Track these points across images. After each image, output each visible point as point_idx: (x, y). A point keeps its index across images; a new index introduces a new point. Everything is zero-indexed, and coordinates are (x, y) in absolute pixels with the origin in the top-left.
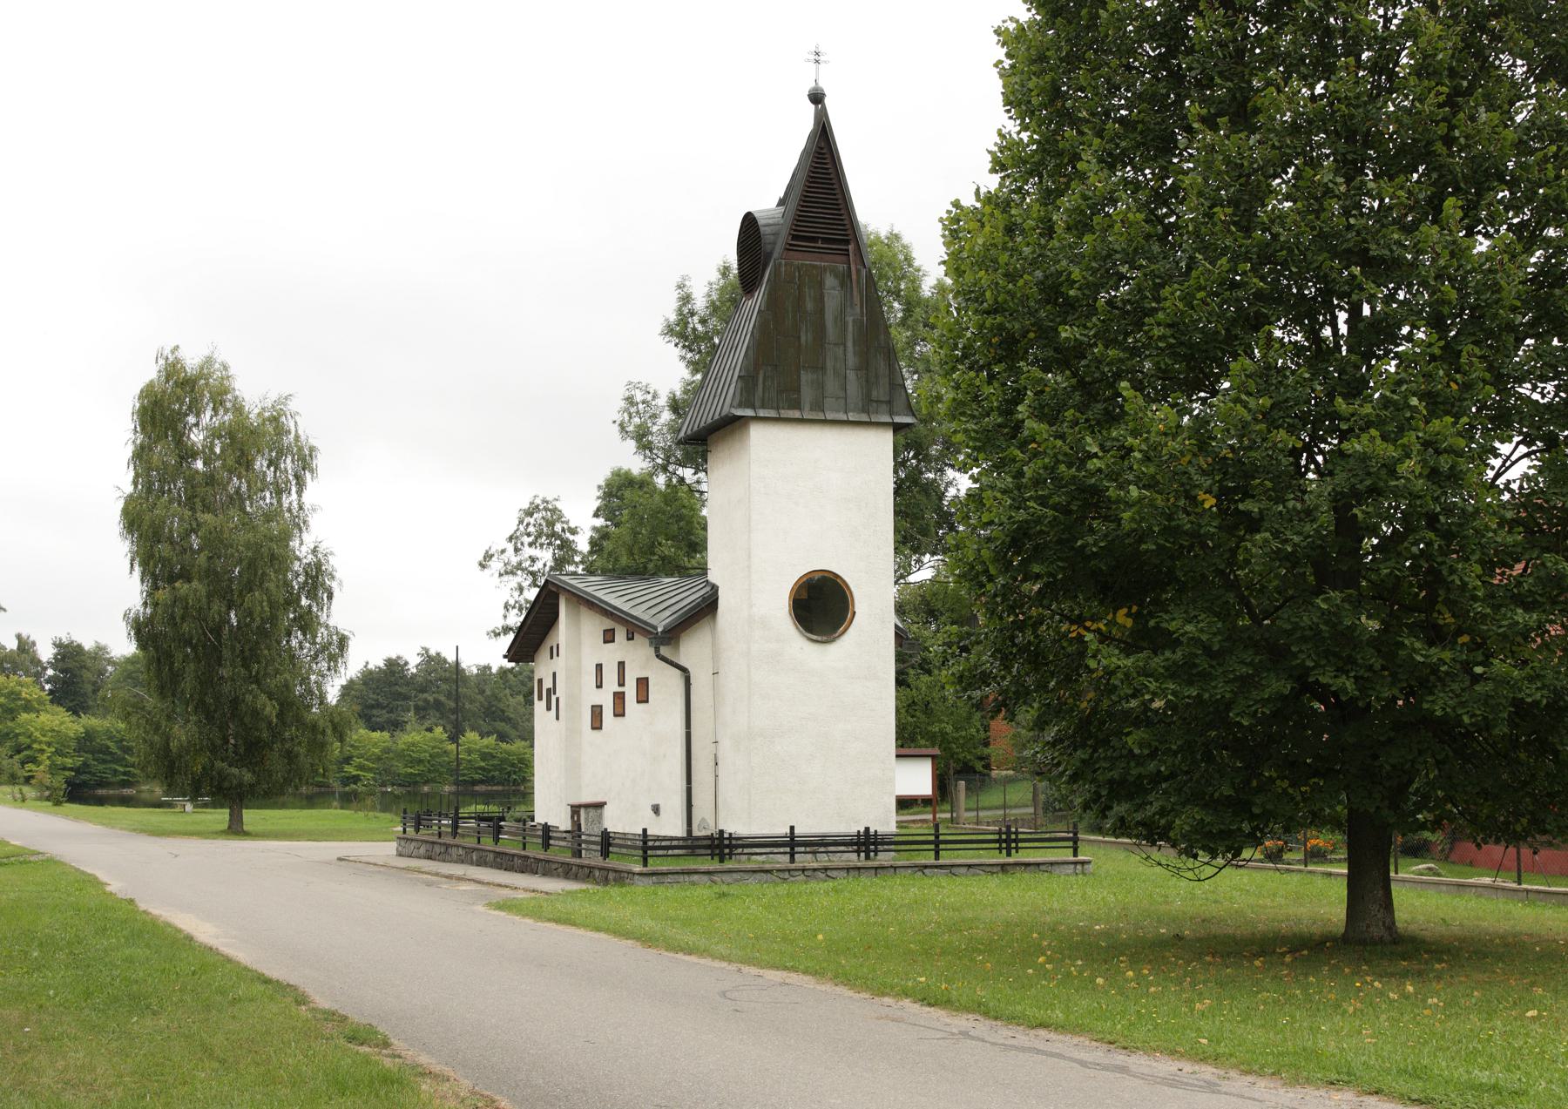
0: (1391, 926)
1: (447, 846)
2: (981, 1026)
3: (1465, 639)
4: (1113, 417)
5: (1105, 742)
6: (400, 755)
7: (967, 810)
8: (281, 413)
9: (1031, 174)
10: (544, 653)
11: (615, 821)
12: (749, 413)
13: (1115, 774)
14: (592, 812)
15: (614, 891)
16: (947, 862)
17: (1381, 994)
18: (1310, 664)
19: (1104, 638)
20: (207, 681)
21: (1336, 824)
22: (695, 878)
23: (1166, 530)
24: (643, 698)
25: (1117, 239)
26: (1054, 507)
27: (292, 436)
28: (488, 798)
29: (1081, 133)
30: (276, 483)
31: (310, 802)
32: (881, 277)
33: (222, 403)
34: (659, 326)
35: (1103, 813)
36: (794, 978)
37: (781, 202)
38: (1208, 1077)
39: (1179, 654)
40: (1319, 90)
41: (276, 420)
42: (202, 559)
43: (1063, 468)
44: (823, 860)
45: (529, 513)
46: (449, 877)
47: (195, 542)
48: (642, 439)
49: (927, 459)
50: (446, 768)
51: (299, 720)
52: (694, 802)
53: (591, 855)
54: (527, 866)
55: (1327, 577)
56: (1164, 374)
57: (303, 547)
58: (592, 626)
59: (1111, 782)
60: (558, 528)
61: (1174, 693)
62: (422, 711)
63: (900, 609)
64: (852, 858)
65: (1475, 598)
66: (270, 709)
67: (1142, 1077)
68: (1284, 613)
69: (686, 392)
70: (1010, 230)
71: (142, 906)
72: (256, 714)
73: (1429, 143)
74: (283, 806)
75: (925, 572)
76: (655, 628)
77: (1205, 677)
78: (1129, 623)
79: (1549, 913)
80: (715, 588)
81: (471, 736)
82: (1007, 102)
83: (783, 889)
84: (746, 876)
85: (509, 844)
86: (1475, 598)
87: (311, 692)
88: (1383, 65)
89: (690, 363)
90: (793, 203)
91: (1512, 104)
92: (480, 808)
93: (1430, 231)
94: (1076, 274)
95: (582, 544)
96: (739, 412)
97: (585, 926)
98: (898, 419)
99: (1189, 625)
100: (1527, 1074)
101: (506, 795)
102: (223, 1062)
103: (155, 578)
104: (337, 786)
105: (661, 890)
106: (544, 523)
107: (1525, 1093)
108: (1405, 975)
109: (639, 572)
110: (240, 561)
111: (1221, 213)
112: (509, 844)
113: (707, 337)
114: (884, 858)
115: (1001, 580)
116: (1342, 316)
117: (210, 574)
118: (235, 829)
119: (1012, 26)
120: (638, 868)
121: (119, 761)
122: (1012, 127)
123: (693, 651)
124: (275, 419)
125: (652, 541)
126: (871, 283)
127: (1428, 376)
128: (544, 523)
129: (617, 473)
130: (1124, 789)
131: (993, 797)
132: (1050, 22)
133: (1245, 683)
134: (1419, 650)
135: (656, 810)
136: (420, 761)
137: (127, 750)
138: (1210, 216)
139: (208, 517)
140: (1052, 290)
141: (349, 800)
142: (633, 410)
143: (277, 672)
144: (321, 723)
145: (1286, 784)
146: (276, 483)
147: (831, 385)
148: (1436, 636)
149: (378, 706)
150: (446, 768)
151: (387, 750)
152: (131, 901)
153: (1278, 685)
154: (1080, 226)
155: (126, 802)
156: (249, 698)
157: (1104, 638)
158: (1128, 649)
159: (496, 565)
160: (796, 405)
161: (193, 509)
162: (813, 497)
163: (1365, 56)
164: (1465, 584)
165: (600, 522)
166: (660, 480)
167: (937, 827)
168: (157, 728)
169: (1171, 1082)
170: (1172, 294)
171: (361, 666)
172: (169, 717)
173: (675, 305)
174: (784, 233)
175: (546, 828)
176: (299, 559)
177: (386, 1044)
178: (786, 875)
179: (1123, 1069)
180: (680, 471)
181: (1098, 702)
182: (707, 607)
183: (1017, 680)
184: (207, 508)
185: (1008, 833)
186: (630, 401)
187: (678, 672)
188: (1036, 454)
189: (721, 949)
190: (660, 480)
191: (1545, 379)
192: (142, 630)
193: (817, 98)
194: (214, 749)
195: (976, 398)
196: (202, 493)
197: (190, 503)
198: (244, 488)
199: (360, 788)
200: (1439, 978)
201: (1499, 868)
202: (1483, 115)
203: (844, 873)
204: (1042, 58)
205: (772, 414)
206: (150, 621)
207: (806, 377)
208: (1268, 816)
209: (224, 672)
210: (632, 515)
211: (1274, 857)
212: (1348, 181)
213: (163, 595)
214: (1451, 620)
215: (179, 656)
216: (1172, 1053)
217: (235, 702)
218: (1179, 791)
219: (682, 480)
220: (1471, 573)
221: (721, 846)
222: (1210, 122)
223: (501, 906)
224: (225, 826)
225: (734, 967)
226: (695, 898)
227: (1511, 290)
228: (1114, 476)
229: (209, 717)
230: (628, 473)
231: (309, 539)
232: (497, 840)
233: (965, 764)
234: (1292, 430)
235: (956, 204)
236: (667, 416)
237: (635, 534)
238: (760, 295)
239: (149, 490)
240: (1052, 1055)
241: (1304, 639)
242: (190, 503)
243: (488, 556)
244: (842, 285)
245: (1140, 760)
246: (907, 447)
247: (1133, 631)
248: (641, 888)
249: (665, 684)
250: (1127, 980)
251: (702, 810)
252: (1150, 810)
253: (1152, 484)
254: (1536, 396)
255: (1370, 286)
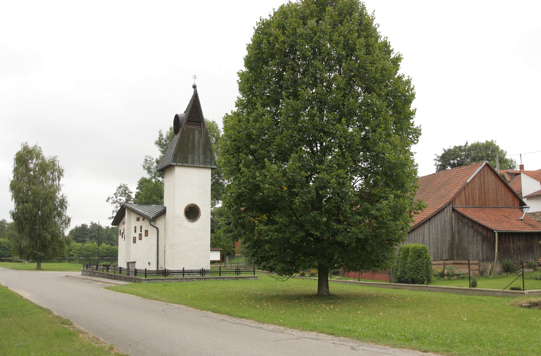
0: (328, 292)
1: (95, 273)
2: (227, 318)
3: (346, 223)
4: (263, 167)
5: (260, 247)
6: (85, 249)
8: (55, 160)
9: (245, 108)
10: (121, 224)
11: (138, 266)
12: (175, 164)
13: (262, 255)
14: (132, 264)
15: (137, 284)
17: (325, 308)
18: (309, 229)
19: (260, 222)
20: (32, 229)
21: (314, 267)
23: (274, 196)
24: (146, 235)
25: (265, 125)
26: (248, 189)
28: (108, 260)
29: (257, 98)
30: (52, 178)
31: (60, 261)
32: (210, 131)
33: (39, 157)
34: (154, 142)
35: (260, 264)
36: (181, 306)
37: (185, 112)
38: (282, 329)
39: (278, 226)
40: (314, 91)
41: (53, 163)
42: (31, 198)
43: (250, 179)
44: (192, 276)
45: (120, 188)
46: (95, 281)
47: (30, 193)
48: (149, 170)
49: (221, 177)
50: (96, 252)
51: (57, 240)
52: (159, 261)
53: (132, 275)
54: (115, 278)
55: (314, 208)
56: (276, 158)
57: (59, 195)
58: (134, 217)
59: (261, 257)
60: (127, 192)
61: (277, 236)
62: (91, 238)
63: (213, 214)
64: (199, 276)
65: (348, 213)
66: (49, 237)
67: (266, 330)
68: (303, 216)
69: (160, 158)
70: (239, 121)
71: (10, 289)
72: (45, 238)
73: (339, 105)
74: (53, 262)
75: (219, 205)
77: (284, 232)
78: (266, 218)
79: (365, 288)
80: (165, 208)
81: (104, 245)
82: (240, 90)
83: (181, 284)
85: (111, 272)
86: (348, 213)
87: (60, 233)
88: (329, 87)
89: (162, 151)
90: (188, 113)
91: (358, 98)
92: (105, 263)
93: (339, 126)
94: (254, 132)
95: (133, 196)
96: (173, 164)
97: (129, 293)
98: (212, 167)
99: (281, 219)
100: (357, 327)
101: (112, 259)
102: (26, 330)
103: (18, 202)
104: (67, 257)
105: (150, 284)
106: (124, 190)
107: (356, 331)
108: (331, 303)
109: (147, 204)
110: (42, 198)
111: (290, 119)
112: (111, 272)
113: (166, 145)
114: (207, 276)
115: (235, 207)
116: (319, 145)
117: (34, 202)
118: (39, 268)
119: (241, 72)
120: (144, 278)
121: (8, 250)
122: (241, 96)
123: (159, 223)
124: (53, 162)
125: (151, 195)
126: (206, 131)
127: (338, 160)
128: (124, 190)
129: (143, 178)
130: (263, 259)
131: (235, 261)
132: (250, 72)
133: (294, 233)
134: (335, 226)
135: (149, 263)
136: (90, 251)
137: (10, 247)
138: (287, 120)
139: (34, 187)
140: (249, 136)
141: (70, 261)
143: (51, 227)
144: (63, 241)
145: (303, 258)
146: (52, 178)
147: (196, 158)
148: (339, 222)
149: (79, 236)
150: (96, 252)
151: (82, 248)
152: (7, 287)
153: (302, 234)
154: (256, 121)
155: (10, 261)
156: (43, 234)
157: (260, 222)
158: (266, 224)
159: (111, 201)
160: (187, 162)
161: (30, 185)
162: (191, 185)
163: (324, 84)
164: (345, 210)
165: (138, 191)
166: (154, 180)
167: (220, 268)
168: (18, 241)
169: (273, 331)
170: (278, 138)
171: (75, 226)
172: (21, 239)
173: (158, 137)
174: (185, 120)
175: (121, 268)
177: (72, 324)
179: (261, 328)
180: (158, 178)
181: (259, 237)
182: (163, 212)
183: (238, 232)
184: (33, 184)
185: (238, 269)
186: (146, 160)
188: (244, 176)
189: (164, 299)
190: (154, 180)
191: (365, 162)
192: (14, 215)
193: (194, 87)
194: (33, 247)
195: (229, 162)
196: (32, 181)
197: (29, 183)
198: (44, 179)
199: (73, 258)
200: (339, 304)
201: (355, 278)
202: (351, 100)
204: (248, 80)
205: (181, 164)
206: (17, 213)
207: (190, 156)
208: (299, 266)
209: (37, 227)
210: (146, 189)
211: (303, 275)
212: (320, 113)
213: (21, 207)
214: (342, 218)
215: (24, 223)
216: (274, 324)
217: (40, 235)
218: (278, 259)
219: (159, 180)
220: (347, 207)
221: (165, 273)
222: (288, 97)
223: (107, 288)
224: (36, 267)
225: (166, 303)
226: (159, 286)
227: (357, 140)
228: (262, 182)
229: (32, 239)
230: (146, 178)
231: (61, 193)
232: (108, 271)
234: (306, 172)
235: (227, 114)
236: (155, 164)
237: (147, 194)
238: (179, 135)
239: (18, 179)
240: (244, 325)
241: (308, 223)
242: (29, 183)
243: (109, 199)
244: (200, 133)
245: (268, 252)
246: (216, 174)
247: (267, 221)
248: (144, 284)
249: (152, 232)
250: (265, 306)
251: (161, 264)
252: (271, 264)
253: (271, 184)
254: (363, 166)
255: (325, 138)
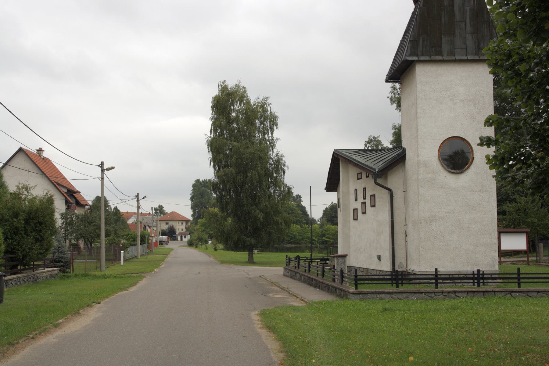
7: (545, 256)
14: (340, 260)
16: (525, 289)
22: (383, 296)
24: (373, 206)
27: (269, 113)
57: (273, 154)
58: (353, 172)
66: (260, 216)
76: (375, 170)
80: (404, 150)
84: (410, 295)
114: (490, 287)
118: (251, 261)
120: (352, 290)
123: (394, 181)
124: (262, 106)
135: (379, 258)
142: (395, 92)
156: (253, 211)
160: (440, 53)
176: (272, 159)
178: (433, 295)
187: (387, 191)
203: (465, 295)
205: (427, 58)
207: (444, 39)
221: (399, 277)
224: (247, 260)
233: (544, 236)
249: (382, 197)
